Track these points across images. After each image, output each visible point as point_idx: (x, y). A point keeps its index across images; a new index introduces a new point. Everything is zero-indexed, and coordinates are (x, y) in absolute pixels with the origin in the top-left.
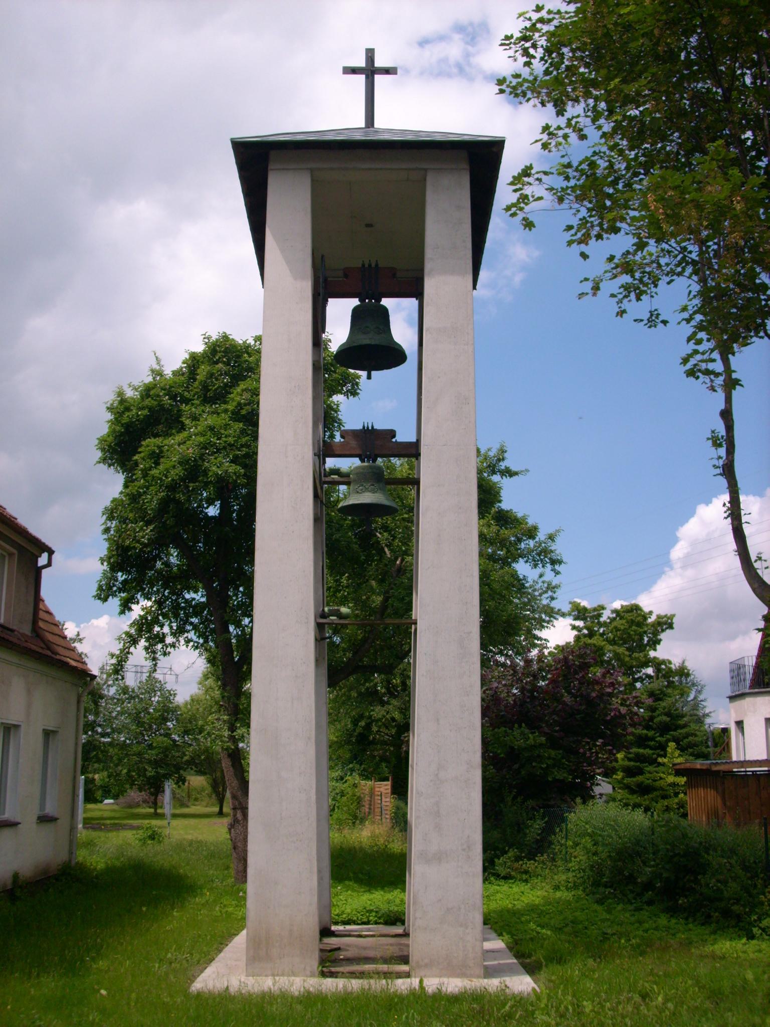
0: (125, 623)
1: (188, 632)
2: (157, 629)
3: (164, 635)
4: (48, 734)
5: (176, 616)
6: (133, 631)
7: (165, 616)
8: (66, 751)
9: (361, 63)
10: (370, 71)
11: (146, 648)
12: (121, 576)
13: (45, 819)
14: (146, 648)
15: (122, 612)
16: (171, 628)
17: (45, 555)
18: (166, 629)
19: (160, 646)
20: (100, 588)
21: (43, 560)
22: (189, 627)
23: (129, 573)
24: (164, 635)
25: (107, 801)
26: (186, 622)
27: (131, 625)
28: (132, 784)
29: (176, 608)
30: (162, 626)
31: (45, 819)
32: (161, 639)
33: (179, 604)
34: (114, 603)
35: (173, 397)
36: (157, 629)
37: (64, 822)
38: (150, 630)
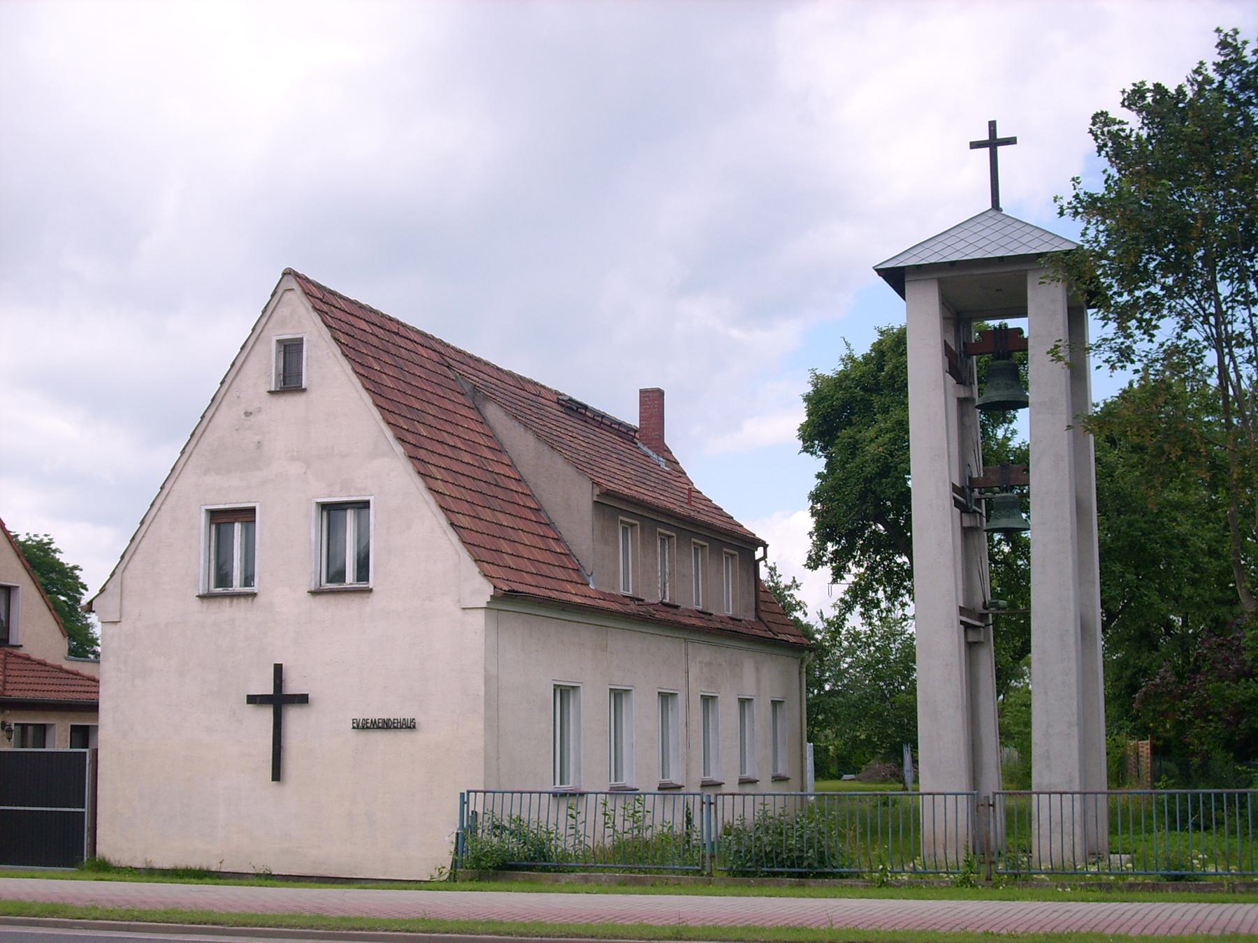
0: (840, 589)
1: (902, 595)
2: (871, 594)
3: (879, 601)
4: (775, 703)
5: (890, 581)
6: (847, 598)
7: (879, 581)
8: (794, 715)
9: (291, 688)
10: (993, 143)
11: (862, 614)
12: (831, 547)
13: (778, 779)
14: (862, 614)
15: (834, 581)
16: (885, 592)
17: (761, 549)
18: (881, 595)
19: (875, 611)
20: (810, 558)
21: (759, 553)
22: (903, 591)
23: (838, 543)
24: (879, 601)
25: (845, 777)
26: (900, 586)
27: (846, 593)
28: (874, 753)
29: (889, 573)
30: (876, 591)
31: (778, 779)
32: (877, 604)
33: (891, 569)
34: (826, 572)
35: (864, 389)
36: (871, 594)
37: (795, 781)
38: (864, 596)
